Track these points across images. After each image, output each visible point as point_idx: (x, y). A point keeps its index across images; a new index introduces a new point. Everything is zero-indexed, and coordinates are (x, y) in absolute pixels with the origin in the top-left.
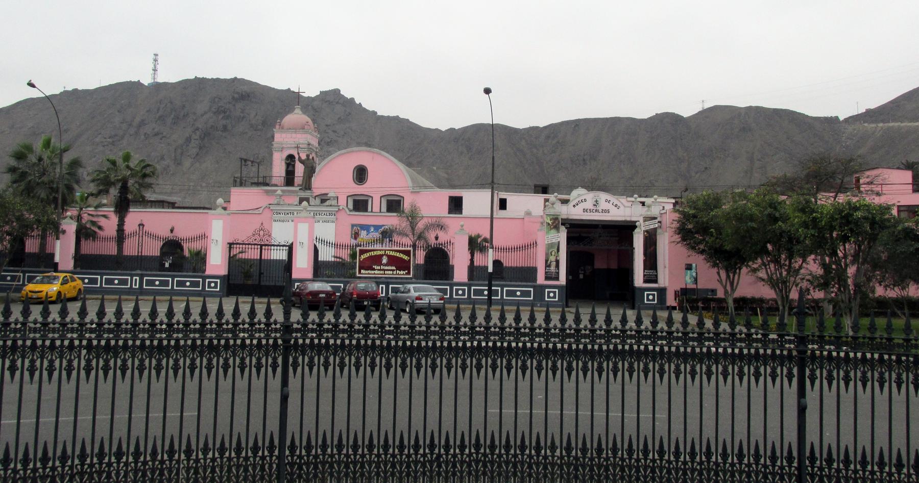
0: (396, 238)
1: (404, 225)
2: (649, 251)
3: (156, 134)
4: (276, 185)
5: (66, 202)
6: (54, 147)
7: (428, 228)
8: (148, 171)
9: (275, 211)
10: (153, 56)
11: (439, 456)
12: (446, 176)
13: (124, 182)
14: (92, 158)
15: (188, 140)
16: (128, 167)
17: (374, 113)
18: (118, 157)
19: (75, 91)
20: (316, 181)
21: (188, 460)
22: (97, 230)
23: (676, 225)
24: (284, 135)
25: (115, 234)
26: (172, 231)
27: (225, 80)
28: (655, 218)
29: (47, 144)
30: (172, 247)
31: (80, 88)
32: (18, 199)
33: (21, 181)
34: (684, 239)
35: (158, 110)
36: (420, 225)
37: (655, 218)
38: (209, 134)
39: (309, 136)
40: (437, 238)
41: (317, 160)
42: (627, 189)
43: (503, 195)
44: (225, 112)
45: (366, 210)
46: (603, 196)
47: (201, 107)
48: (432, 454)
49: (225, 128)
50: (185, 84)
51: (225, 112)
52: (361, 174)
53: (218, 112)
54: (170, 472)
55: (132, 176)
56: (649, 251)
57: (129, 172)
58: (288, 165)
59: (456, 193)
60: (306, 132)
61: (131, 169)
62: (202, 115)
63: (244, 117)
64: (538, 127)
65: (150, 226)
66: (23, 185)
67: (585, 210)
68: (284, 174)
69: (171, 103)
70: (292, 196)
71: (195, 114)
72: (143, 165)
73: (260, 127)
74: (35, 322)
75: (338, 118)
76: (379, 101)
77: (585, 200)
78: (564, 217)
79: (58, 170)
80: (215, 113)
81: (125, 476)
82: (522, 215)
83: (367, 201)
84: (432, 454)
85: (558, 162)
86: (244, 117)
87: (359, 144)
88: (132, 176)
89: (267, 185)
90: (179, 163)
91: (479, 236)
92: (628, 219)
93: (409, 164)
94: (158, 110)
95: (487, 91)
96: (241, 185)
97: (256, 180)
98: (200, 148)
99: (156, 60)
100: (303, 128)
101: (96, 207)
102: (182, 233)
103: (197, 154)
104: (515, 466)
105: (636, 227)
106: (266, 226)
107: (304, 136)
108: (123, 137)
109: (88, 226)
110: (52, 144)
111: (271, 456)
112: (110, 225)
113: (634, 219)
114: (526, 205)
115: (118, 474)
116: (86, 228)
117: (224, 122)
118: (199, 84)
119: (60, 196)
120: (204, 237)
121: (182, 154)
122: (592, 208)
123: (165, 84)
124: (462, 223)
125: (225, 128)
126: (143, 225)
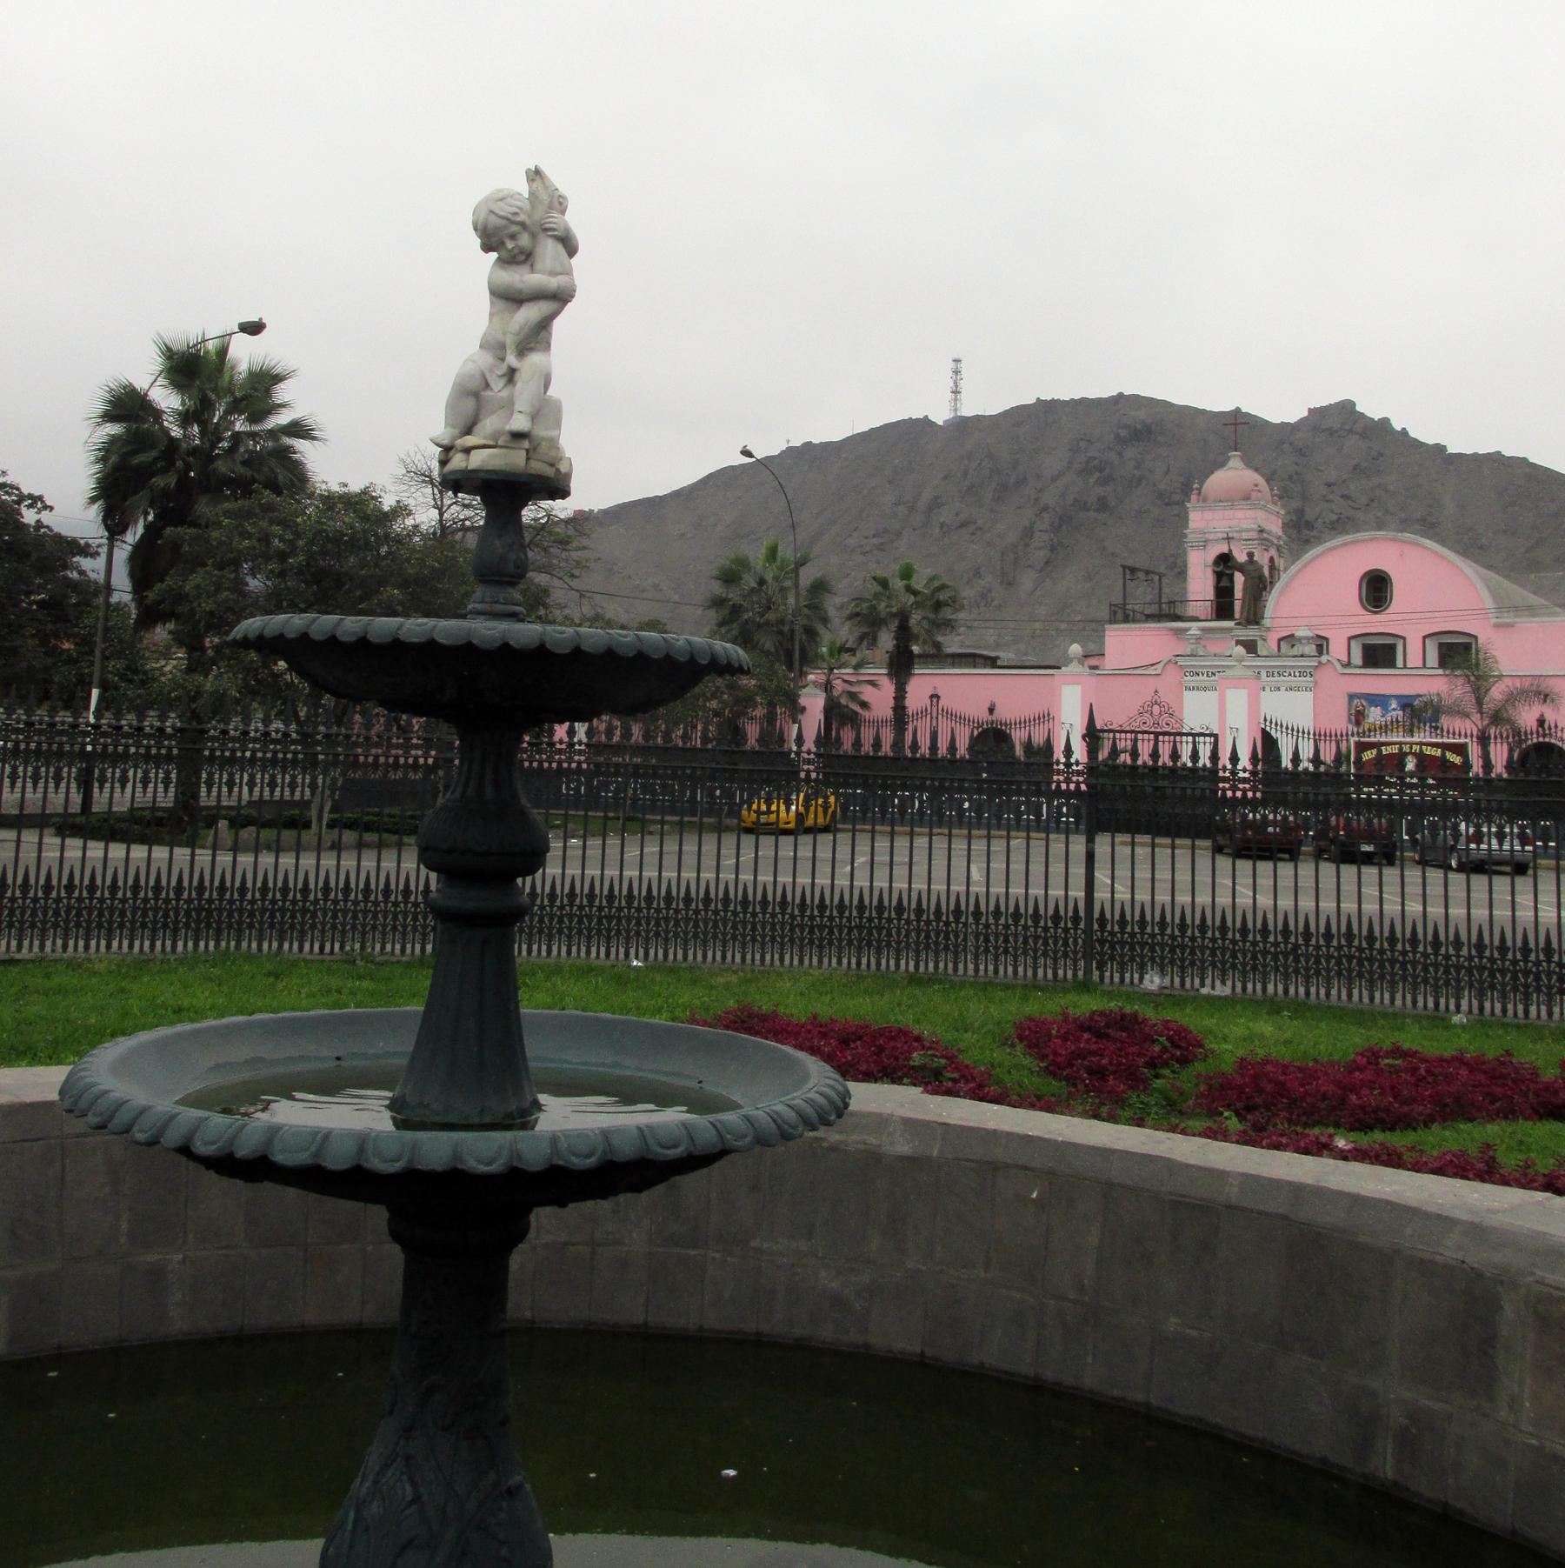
0: (1445, 721)
1: (1457, 693)
5: (808, 659)
6: (783, 561)
7: (1512, 698)
8: (943, 596)
9: (1189, 669)
10: (952, 365)
13: (903, 617)
15: (1028, 533)
16: (910, 590)
17: (1440, 449)
18: (890, 570)
19: (808, 446)
20: (1274, 604)
21: (977, 924)
24: (1208, 515)
25: (889, 713)
26: (991, 711)
27: (1099, 402)
29: (772, 553)
30: (993, 737)
31: (816, 441)
33: (732, 622)
35: (966, 473)
36: (1497, 693)
39: (1260, 514)
40: (1541, 722)
41: (1280, 563)
45: (1392, 665)
48: (1286, 943)
49: (1103, 504)
50: (1018, 416)
51: (1101, 470)
52: (1376, 589)
53: (1085, 471)
54: (957, 937)
55: (917, 605)
57: (912, 598)
58: (1219, 576)
60: (1255, 507)
61: (915, 593)
62: (1054, 479)
63: (1140, 479)
65: (954, 700)
70: (1226, 640)
72: (936, 584)
73: (1176, 497)
74: (809, 752)
75: (1344, 469)
76: (1447, 415)
79: (791, 600)
80: (1079, 473)
81: (907, 936)
83: (1392, 648)
84: (1286, 943)
86: (1140, 479)
87: (1405, 525)
88: (917, 605)
89: (1178, 618)
90: (1010, 584)
94: (966, 473)
96: (1126, 620)
97: (1153, 610)
98: (1053, 549)
99: (957, 372)
100: (1247, 498)
102: (1005, 713)
103: (1047, 563)
106: (1164, 697)
107: (1250, 513)
108: (899, 534)
109: (843, 701)
110: (780, 554)
111: (1076, 929)
112: (880, 699)
115: (899, 933)
116: (839, 705)
117: (1100, 491)
119: (795, 649)
120: (1046, 717)
121: (1016, 561)
123: (978, 418)
125: (1103, 504)
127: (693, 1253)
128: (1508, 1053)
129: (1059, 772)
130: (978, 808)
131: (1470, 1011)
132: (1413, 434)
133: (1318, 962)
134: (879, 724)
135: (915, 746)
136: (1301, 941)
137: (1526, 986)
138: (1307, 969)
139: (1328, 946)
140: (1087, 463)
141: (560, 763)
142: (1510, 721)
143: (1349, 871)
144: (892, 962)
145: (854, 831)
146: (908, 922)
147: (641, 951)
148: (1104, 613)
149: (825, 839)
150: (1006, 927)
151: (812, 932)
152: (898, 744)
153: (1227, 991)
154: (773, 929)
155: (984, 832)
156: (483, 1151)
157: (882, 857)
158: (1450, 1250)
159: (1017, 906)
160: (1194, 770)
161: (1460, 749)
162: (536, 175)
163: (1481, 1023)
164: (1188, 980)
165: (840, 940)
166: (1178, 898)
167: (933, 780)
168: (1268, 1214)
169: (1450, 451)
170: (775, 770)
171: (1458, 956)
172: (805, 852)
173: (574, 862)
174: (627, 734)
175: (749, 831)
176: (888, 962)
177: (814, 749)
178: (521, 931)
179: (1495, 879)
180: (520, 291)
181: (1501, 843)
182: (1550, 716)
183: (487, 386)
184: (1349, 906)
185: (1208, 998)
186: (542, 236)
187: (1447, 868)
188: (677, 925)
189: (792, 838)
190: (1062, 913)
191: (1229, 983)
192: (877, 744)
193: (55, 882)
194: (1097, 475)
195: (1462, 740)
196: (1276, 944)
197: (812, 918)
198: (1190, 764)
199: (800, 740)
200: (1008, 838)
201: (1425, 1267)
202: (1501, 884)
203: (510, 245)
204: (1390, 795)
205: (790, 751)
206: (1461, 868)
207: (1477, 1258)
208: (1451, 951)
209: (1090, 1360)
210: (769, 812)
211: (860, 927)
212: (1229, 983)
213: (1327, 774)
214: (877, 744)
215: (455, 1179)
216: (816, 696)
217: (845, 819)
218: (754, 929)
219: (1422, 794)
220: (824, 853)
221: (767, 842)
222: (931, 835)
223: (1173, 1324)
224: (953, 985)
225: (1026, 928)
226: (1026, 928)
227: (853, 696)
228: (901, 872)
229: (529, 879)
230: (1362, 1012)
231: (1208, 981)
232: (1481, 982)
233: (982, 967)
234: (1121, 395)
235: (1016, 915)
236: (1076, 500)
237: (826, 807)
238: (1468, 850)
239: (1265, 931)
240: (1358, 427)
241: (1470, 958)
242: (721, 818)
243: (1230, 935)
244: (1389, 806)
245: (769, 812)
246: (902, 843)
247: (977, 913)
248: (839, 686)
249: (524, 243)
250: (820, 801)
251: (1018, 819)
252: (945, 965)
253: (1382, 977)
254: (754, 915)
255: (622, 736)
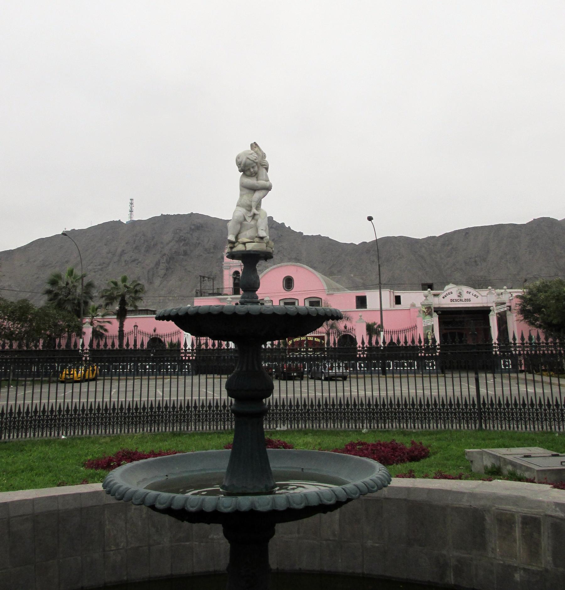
2: (502, 328)
3: (134, 261)
4: (227, 295)
8: (138, 288)
11: (309, 410)
12: (361, 281)
13: (123, 296)
14: (102, 283)
15: (158, 264)
16: (125, 286)
21: (195, 411)
22: (104, 332)
23: (518, 308)
25: (117, 334)
26: (155, 331)
28: (504, 303)
29: (71, 273)
32: (55, 311)
34: (526, 318)
35: (135, 241)
37: (504, 303)
38: (174, 258)
40: (345, 327)
42: (479, 284)
43: (397, 293)
44: (185, 240)
46: (465, 289)
47: (167, 238)
48: (305, 409)
49: (185, 253)
51: (185, 240)
52: (289, 283)
53: (180, 240)
54: (188, 416)
55: (129, 292)
56: (502, 328)
59: (361, 293)
61: (128, 287)
62: (168, 244)
64: (435, 237)
66: (56, 302)
67: (452, 300)
68: (232, 286)
69: (144, 235)
71: (162, 243)
73: (212, 250)
77: (452, 293)
78: (436, 306)
80: (177, 242)
81: (169, 418)
82: (408, 307)
84: (305, 409)
85: (454, 264)
86: (199, 243)
87: (290, 260)
89: (220, 294)
91: (375, 324)
92: (485, 305)
93: (324, 273)
94: (135, 241)
95: (370, 219)
97: (211, 292)
98: (167, 269)
99: (131, 204)
101: (103, 316)
103: (165, 274)
104: (344, 414)
105: (490, 311)
108: (108, 265)
109: (97, 329)
112: (113, 327)
113: (489, 305)
114: (414, 298)
115: (166, 417)
117: (184, 248)
118: (165, 219)
119: (80, 309)
121: (153, 275)
122: (457, 298)
124: (360, 314)
125: (185, 253)
126: (137, 326)
127: (187, 543)
128: (379, 441)
129: (182, 353)
130: (152, 367)
131: (367, 428)
132: (292, 229)
133: (316, 415)
134: (113, 337)
135: (128, 345)
136: (310, 408)
137: (384, 417)
138: (312, 418)
139: (319, 409)
140: (180, 238)
141: (544, 351)
142: (336, 328)
143: (290, 383)
144: (164, 428)
145: (104, 380)
146: (170, 412)
147: (64, 432)
148: (194, 292)
149: (92, 384)
150: (206, 411)
151: (132, 419)
152: (121, 345)
153: (285, 428)
154: (117, 419)
155: (117, 378)
156: (263, 503)
157: (122, 389)
158: (465, 503)
159: (210, 403)
160: (406, 347)
161: (322, 338)
162: (254, 146)
163: (372, 431)
164: (272, 425)
165: (144, 421)
166: (411, 391)
167: (135, 357)
168: (400, 499)
169: (304, 234)
170: (72, 357)
171: (362, 409)
172: (84, 389)
173: (283, 392)
174: (11, 346)
175: (62, 382)
176: (162, 428)
177: (89, 348)
178: (266, 419)
179: (338, 382)
180: (257, 187)
181: (339, 369)
182: (349, 325)
183: (245, 220)
184: (333, 395)
185: (280, 431)
186: (261, 167)
187: (320, 379)
188: (79, 420)
189: (79, 384)
190: (168, 405)
191: (286, 425)
192: (113, 345)
193: (321, 403)
194: (183, 243)
195: (323, 335)
196: (302, 410)
197: (79, 415)
198: (419, 345)
199: (83, 345)
200: (163, 379)
201: (458, 510)
202: (340, 384)
203: (252, 170)
204: (296, 355)
205: (79, 349)
206: (326, 379)
207: (475, 504)
208: (360, 407)
209: (340, 561)
210: (70, 374)
211: (151, 416)
212: (286, 425)
213: (276, 349)
214: (113, 345)
215: (252, 513)
216: (89, 327)
217: (100, 375)
218: (110, 420)
219: (300, 354)
220: (92, 389)
221: (69, 386)
222: (134, 379)
223: (369, 543)
224: (190, 435)
225: (213, 411)
226: (213, 411)
227: (102, 327)
228: (130, 394)
229: (267, 399)
230: (324, 431)
231: (279, 425)
232: (370, 417)
233: (197, 427)
234: (192, 213)
235: (210, 407)
236: (175, 252)
237: (93, 370)
238: (329, 372)
239: (340, 405)
240: (274, 226)
241: (366, 409)
242: (54, 378)
243: (286, 408)
244: (302, 360)
245: (70, 374)
246: (130, 383)
247: (195, 407)
248: (96, 324)
249: (252, 168)
250: (91, 368)
251: (167, 371)
252: (184, 427)
253: (316, 419)
254: (110, 414)
255: (218, 346)
